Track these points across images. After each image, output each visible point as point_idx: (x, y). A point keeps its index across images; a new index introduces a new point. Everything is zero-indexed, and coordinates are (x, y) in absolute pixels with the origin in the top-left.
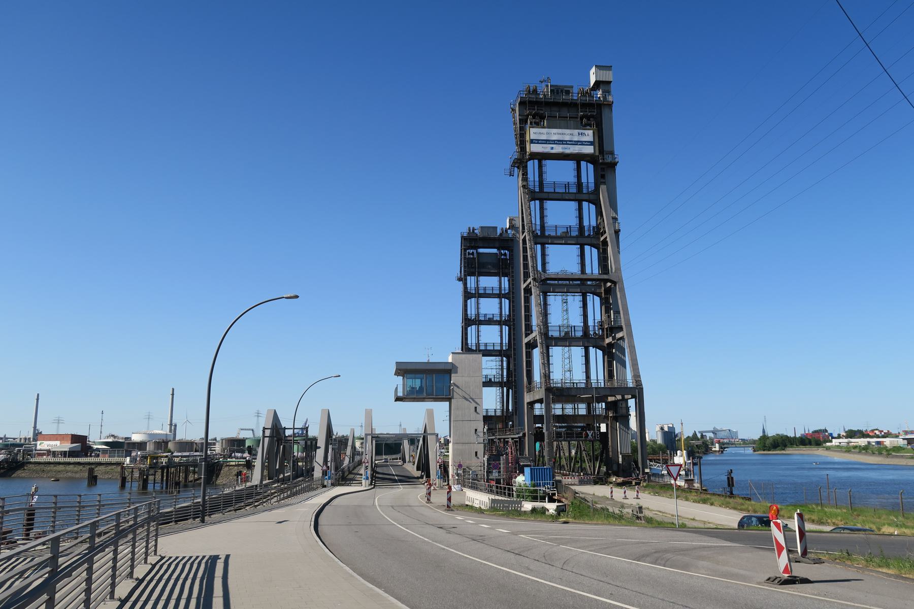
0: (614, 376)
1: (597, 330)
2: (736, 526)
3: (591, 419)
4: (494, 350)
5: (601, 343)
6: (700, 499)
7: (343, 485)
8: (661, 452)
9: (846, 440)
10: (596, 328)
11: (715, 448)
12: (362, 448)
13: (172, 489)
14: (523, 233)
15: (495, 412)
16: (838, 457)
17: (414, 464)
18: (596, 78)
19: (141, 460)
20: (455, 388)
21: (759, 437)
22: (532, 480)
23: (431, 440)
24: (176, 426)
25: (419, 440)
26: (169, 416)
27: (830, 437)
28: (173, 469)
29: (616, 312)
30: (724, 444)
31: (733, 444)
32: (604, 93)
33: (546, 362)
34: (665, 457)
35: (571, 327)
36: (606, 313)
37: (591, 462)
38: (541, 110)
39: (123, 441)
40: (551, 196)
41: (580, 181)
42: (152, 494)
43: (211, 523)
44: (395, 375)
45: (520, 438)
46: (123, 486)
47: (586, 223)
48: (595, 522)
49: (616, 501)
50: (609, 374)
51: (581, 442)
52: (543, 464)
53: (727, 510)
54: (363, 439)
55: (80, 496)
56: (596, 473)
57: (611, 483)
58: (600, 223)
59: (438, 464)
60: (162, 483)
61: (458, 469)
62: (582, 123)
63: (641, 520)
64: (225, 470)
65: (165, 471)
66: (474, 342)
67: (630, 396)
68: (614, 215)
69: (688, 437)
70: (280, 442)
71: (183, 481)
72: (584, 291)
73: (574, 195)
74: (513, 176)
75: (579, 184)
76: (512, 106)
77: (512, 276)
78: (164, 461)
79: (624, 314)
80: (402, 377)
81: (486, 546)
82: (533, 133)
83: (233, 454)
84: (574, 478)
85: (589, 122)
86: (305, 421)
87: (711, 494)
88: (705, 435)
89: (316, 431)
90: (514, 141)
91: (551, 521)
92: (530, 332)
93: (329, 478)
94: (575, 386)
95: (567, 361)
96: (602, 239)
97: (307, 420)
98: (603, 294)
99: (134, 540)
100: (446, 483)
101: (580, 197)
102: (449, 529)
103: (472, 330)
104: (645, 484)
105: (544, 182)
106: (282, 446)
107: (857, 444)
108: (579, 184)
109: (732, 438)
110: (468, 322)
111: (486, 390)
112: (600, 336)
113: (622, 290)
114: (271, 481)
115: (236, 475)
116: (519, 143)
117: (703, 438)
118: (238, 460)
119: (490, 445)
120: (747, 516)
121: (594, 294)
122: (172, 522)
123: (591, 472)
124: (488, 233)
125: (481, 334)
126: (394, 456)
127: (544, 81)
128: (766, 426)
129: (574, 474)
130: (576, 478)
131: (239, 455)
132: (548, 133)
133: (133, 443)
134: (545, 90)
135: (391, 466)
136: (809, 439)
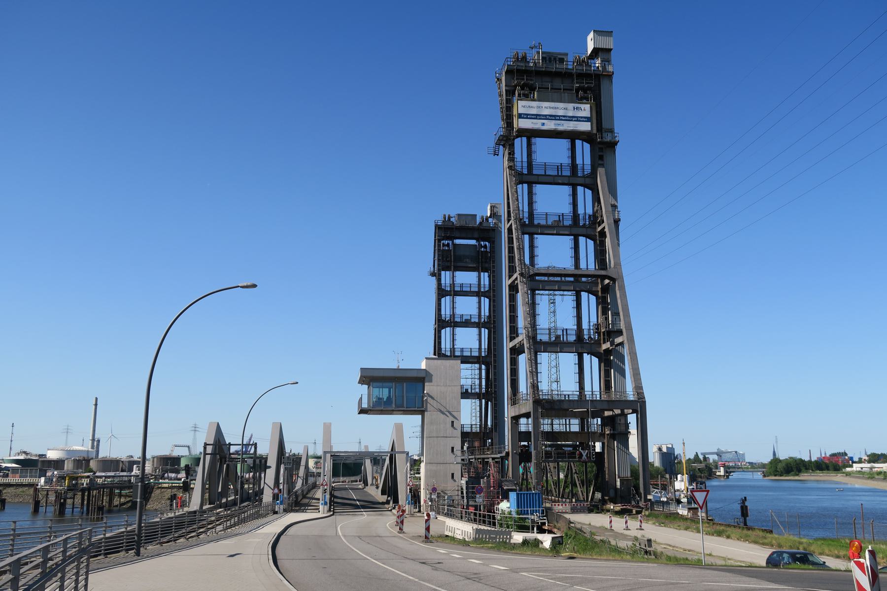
0: (612, 387)
1: (592, 333)
2: (764, 564)
3: (585, 437)
4: (471, 357)
5: (597, 349)
6: (713, 530)
7: (297, 511)
8: (659, 476)
9: (869, 465)
10: (592, 331)
11: (720, 472)
12: (317, 468)
13: (94, 515)
14: (509, 221)
15: (472, 427)
16: (858, 484)
17: (377, 488)
18: (594, 45)
19: (58, 481)
20: (429, 400)
21: (770, 460)
22: (518, 507)
23: (400, 460)
24: (99, 441)
25: (385, 460)
26: (92, 429)
27: (851, 462)
28: (95, 492)
29: (615, 313)
30: (729, 467)
31: (739, 468)
32: (603, 62)
33: (534, 370)
34: (664, 481)
35: (563, 331)
36: (603, 315)
37: (583, 486)
38: (531, 80)
39: (37, 458)
40: (541, 179)
41: (575, 163)
42: (78, 522)
43: (148, 557)
44: (358, 383)
45: (502, 458)
46: (36, 510)
47: (581, 211)
48: (605, 558)
49: (616, 532)
50: (606, 385)
51: (572, 464)
52: (527, 488)
53: (747, 544)
54: (320, 458)
55: (15, 522)
56: (589, 500)
57: (608, 511)
58: (597, 211)
59: (408, 487)
60: (82, 507)
61: (431, 494)
62: (577, 96)
63: (650, 554)
64: (157, 492)
65: (86, 494)
66: (448, 346)
67: (631, 411)
68: (614, 202)
69: (690, 459)
70: (223, 460)
71: (107, 506)
72: (578, 289)
73: (568, 178)
74: (498, 155)
75: (574, 166)
76: (497, 75)
77: (494, 271)
78: (85, 482)
79: (624, 316)
80: (367, 386)
81: (485, 586)
82: (522, 106)
83: (166, 475)
84: (566, 505)
85: (586, 95)
86: (250, 436)
87: (726, 525)
88: (708, 458)
89: (266, 448)
90: (500, 115)
91: (551, 556)
92: (515, 335)
93: (281, 503)
94: (567, 399)
95: (554, 370)
96: (599, 229)
97: (252, 436)
98: (600, 294)
99: (62, 580)
100: (417, 510)
101: (574, 180)
102: (434, 565)
103: (446, 333)
104: (647, 513)
105: (533, 163)
106: (225, 465)
107: (881, 469)
108: (574, 166)
109: (739, 461)
110: (441, 323)
111: (463, 401)
112: (596, 341)
113: (622, 288)
114: (212, 506)
115: (169, 499)
116: (505, 117)
117: (706, 461)
118: (172, 481)
119: (467, 465)
120: (779, 552)
121: (590, 292)
122: (100, 555)
123: (584, 499)
124: (466, 222)
125: (457, 337)
126: (353, 478)
127: (535, 47)
128: (777, 448)
129: (564, 500)
130: (567, 506)
131: (173, 475)
132: (539, 107)
133: (49, 461)
134: (536, 57)
135: (351, 489)
136: (825, 463)
